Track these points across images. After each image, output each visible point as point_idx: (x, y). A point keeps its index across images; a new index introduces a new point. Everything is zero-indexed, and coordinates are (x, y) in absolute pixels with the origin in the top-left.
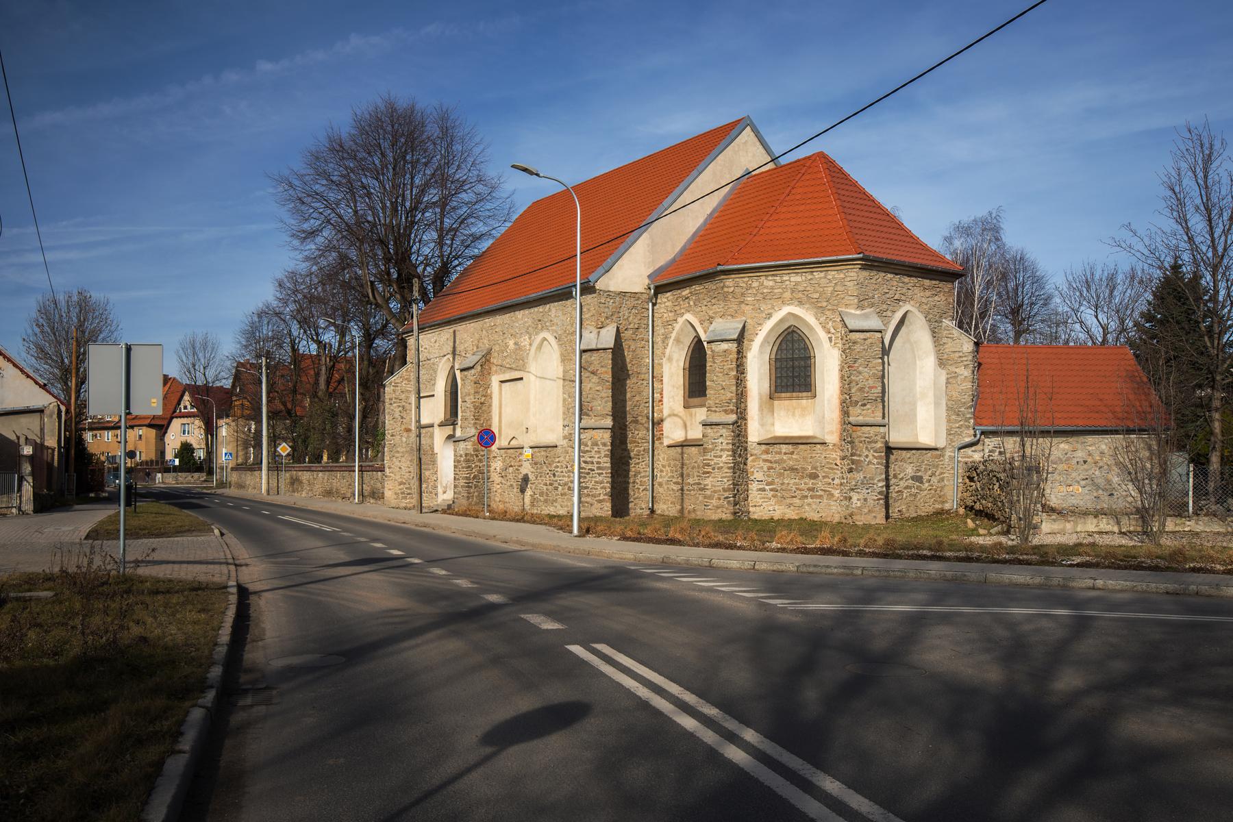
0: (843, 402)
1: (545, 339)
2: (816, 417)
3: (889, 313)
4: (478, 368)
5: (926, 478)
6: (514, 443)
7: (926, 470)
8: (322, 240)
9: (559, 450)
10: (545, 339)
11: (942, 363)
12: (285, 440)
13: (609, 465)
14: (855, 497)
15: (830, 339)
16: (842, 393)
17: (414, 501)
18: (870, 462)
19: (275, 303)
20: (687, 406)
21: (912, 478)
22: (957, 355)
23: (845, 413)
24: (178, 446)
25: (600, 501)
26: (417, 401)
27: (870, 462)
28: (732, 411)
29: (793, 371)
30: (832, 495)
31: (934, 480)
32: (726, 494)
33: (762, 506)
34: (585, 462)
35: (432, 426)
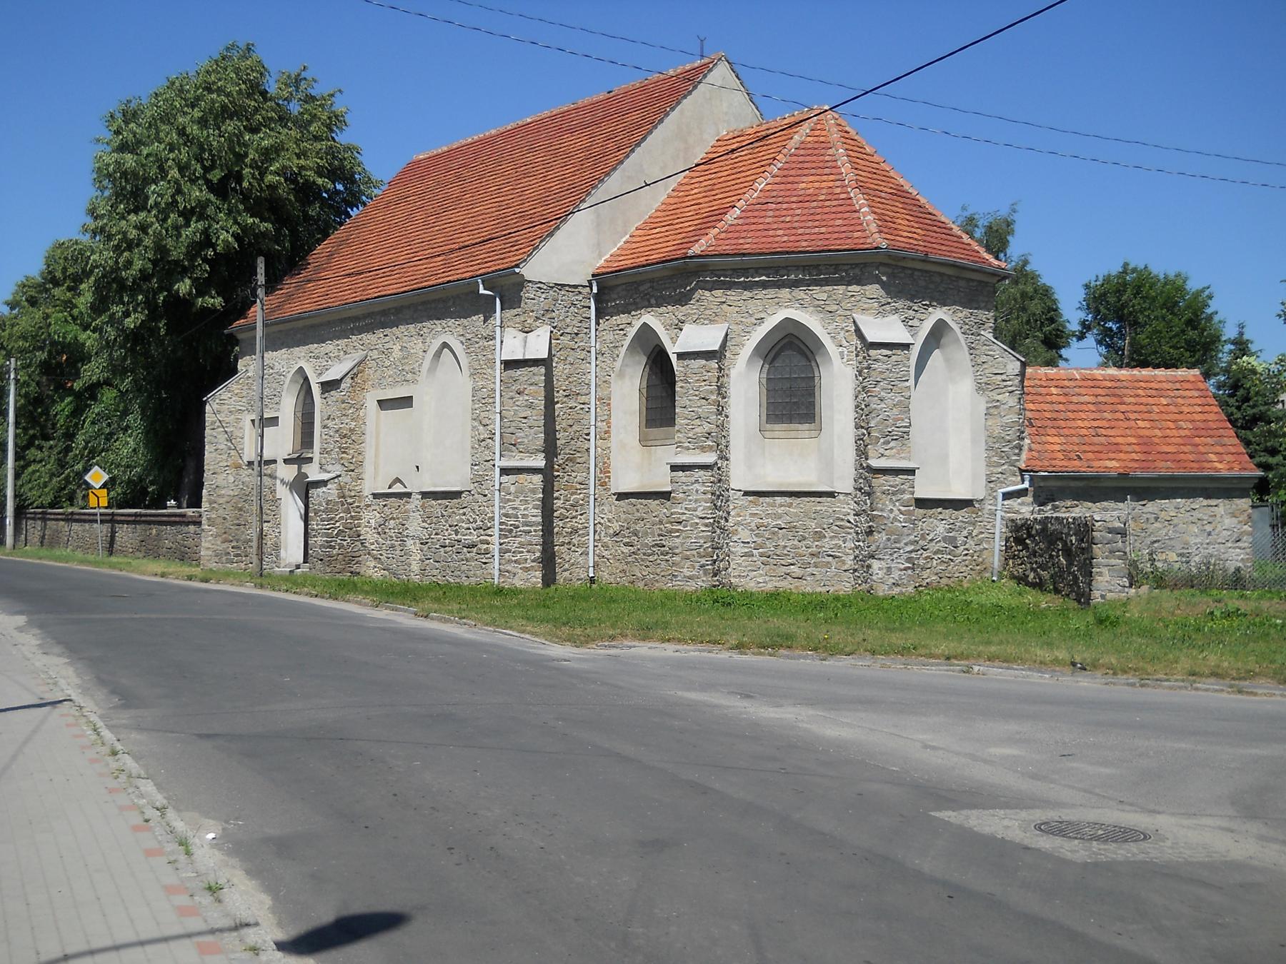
0: (859, 439)
1: (445, 345)
2: (820, 458)
3: (915, 322)
4: (348, 381)
5: (960, 540)
6: (398, 488)
7: (960, 530)
8: (862, 206)
9: (465, 498)
10: (445, 345)
11: (981, 388)
12: (87, 470)
13: (539, 519)
14: (876, 565)
15: (842, 353)
16: (858, 427)
17: (253, 567)
18: (895, 519)
19: (40, 280)
20: (644, 441)
21: (945, 539)
22: (999, 377)
23: (862, 453)
24: (1081, 294)
25: (526, 569)
26: (245, 422)
27: (895, 519)
28: (711, 447)
29: (792, 399)
30: (844, 562)
31: (971, 542)
32: (703, 561)
33: (749, 576)
34: (506, 515)
35: (275, 461)
